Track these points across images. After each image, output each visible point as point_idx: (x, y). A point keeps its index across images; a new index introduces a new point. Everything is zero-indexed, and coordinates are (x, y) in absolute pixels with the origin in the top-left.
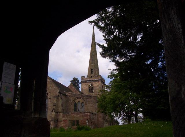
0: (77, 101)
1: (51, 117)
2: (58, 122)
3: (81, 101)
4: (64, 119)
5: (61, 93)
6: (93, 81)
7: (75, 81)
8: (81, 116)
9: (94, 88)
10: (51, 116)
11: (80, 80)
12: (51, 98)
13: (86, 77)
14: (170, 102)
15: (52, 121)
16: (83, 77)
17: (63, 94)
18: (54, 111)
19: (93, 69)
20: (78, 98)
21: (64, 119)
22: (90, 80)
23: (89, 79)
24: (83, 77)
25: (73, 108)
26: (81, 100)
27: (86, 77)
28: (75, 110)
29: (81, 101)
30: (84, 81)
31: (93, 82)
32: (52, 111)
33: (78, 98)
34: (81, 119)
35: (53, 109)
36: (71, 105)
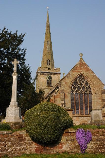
6: (51, 73)
19: (49, 60)
31: (51, 75)
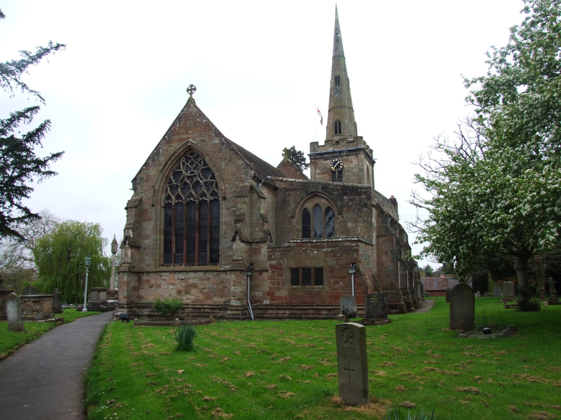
0: (309, 206)
1: (232, 256)
2: (255, 273)
3: (324, 203)
4: (274, 262)
5: (260, 181)
6: (341, 152)
7: (292, 156)
8: (327, 252)
9: (345, 174)
10: (230, 254)
11: (306, 151)
12: (229, 196)
13: (322, 143)
14: (87, 275)
15: (236, 273)
16: (314, 145)
17: (265, 184)
18: (238, 238)
19: (340, 122)
20: (314, 195)
21: (274, 262)
22: (335, 152)
23: (331, 150)
24: (314, 143)
25: (300, 227)
26: (324, 201)
27: (322, 143)
28: (306, 232)
29: (324, 203)
30: (318, 154)
31: (342, 156)
32: (234, 240)
33: (312, 197)
34: (331, 262)
35: (236, 232)
36: (293, 217)
